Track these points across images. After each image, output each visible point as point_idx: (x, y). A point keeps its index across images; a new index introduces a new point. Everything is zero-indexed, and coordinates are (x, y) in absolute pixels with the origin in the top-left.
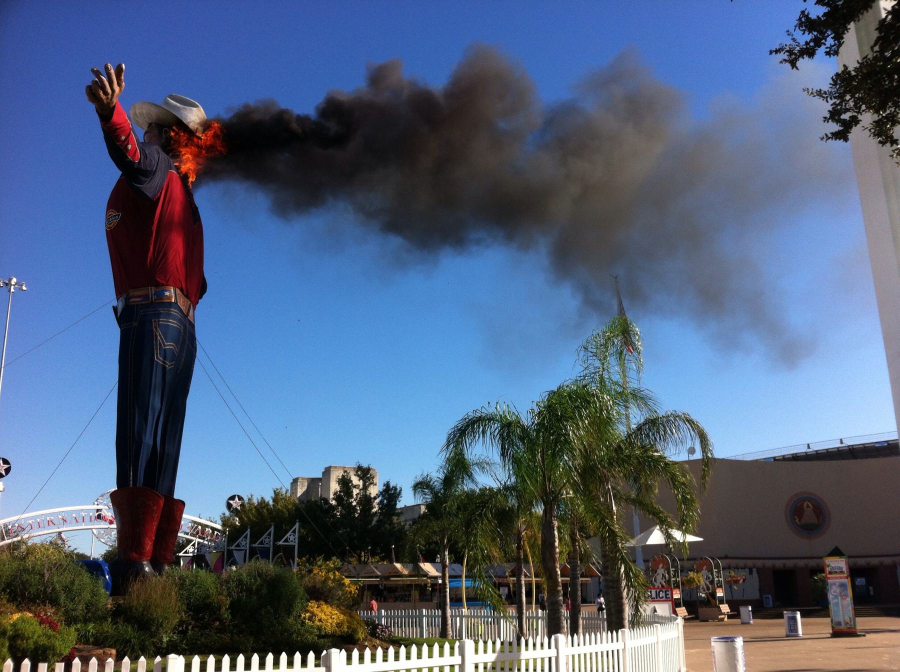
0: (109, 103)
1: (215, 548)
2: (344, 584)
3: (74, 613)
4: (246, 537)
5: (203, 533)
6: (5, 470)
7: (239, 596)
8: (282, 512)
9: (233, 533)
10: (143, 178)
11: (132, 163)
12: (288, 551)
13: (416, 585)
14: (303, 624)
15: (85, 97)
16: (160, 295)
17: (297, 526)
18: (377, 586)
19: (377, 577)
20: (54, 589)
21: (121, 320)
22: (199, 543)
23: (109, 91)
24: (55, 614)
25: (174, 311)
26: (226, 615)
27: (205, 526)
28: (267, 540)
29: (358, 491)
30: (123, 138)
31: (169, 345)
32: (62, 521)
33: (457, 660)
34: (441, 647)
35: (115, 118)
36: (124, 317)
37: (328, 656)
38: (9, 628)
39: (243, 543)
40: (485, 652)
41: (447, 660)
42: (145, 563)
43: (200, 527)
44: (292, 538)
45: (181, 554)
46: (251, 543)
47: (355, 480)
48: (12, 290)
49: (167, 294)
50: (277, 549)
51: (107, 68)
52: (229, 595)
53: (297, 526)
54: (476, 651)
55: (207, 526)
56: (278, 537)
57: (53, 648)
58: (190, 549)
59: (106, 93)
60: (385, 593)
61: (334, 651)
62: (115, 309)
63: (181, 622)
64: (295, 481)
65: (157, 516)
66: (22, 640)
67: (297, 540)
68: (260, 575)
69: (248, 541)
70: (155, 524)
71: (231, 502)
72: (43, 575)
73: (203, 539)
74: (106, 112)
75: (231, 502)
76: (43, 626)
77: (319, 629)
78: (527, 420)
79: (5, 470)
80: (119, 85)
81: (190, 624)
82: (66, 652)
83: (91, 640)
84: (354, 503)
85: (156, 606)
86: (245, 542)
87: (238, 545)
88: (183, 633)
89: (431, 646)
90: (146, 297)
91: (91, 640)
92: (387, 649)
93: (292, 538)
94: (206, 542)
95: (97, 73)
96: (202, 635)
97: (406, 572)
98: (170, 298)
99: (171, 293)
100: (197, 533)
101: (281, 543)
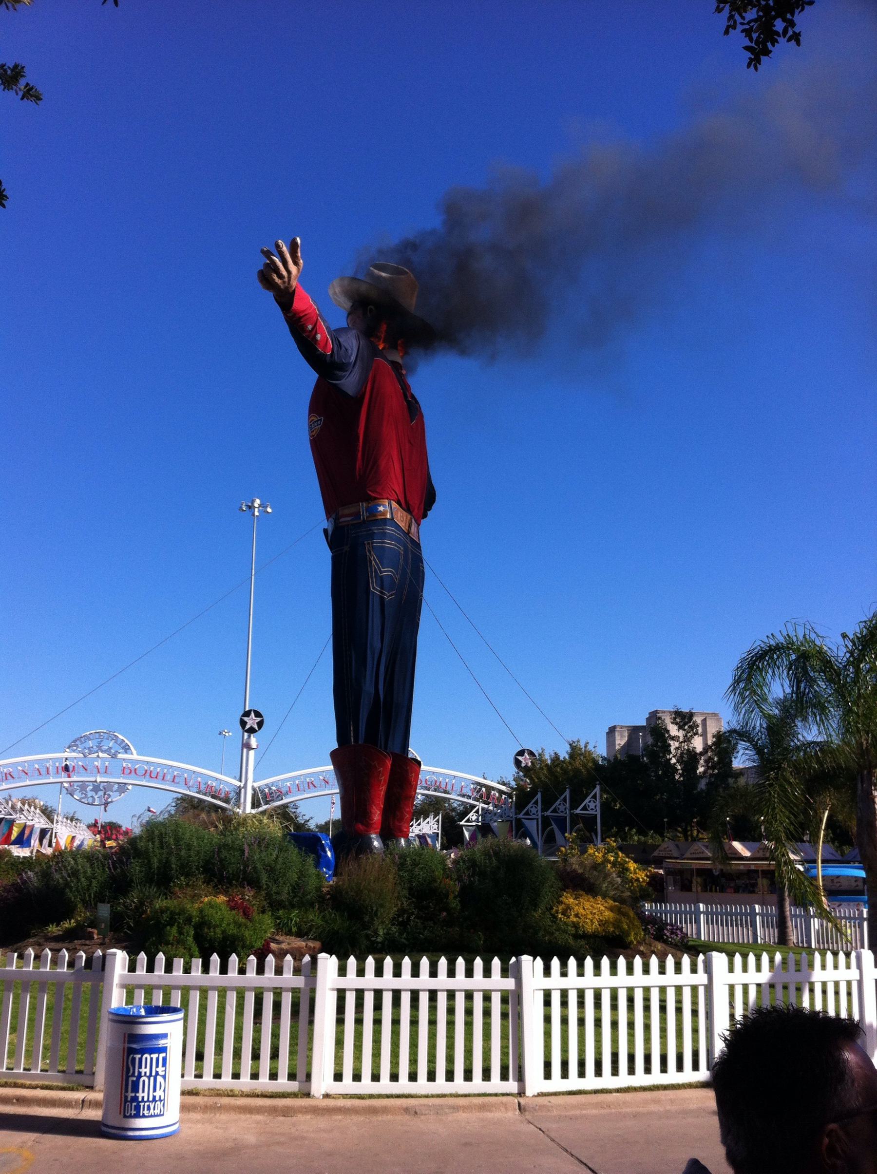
0: (287, 288)
1: (501, 817)
2: (627, 869)
3: (278, 898)
4: (536, 803)
5: (488, 797)
6: (258, 723)
7: (470, 880)
8: (581, 772)
9: (522, 797)
10: (340, 373)
11: (324, 355)
12: (590, 822)
13: (763, 872)
14: (555, 917)
15: (258, 285)
16: (373, 511)
17: (597, 789)
18: (710, 870)
19: (707, 859)
20: (255, 868)
21: (332, 544)
22: (483, 809)
23: (285, 273)
24: (254, 897)
25: (389, 529)
26: (454, 904)
27: (489, 788)
28: (562, 807)
29: (677, 744)
30: (310, 327)
31: (387, 572)
32: (323, 783)
33: (701, 978)
34: (564, 964)
35: (297, 305)
36: (336, 539)
37: (518, 963)
38: (195, 913)
39: (534, 810)
40: (836, 967)
41: (686, 978)
42: (373, 836)
43: (484, 789)
44: (593, 805)
45: (462, 823)
46: (543, 810)
47: (673, 730)
48: (257, 513)
49: (381, 508)
50: (575, 819)
51: (278, 246)
52: (460, 879)
53: (597, 789)
54: (731, 970)
55: (493, 789)
56: (574, 805)
57: (242, 939)
58: (472, 816)
59: (281, 276)
60: (723, 880)
61: (526, 959)
62: (325, 531)
63: (402, 912)
64: (612, 730)
65: (384, 779)
66: (209, 928)
67: (598, 808)
68: (496, 854)
69: (568, 805)
70: (383, 789)
71: (520, 758)
72: (243, 851)
73: (488, 804)
74: (285, 298)
75: (520, 758)
76: (234, 912)
77: (575, 926)
78: (838, 649)
79: (258, 723)
80: (296, 263)
81: (413, 913)
82: (259, 944)
83: (294, 929)
84: (673, 761)
85: (369, 891)
86: (535, 809)
87: (527, 813)
88: (404, 925)
89: (745, 956)
90: (357, 515)
91: (294, 929)
92: (761, 956)
93: (593, 805)
94: (491, 808)
95: (268, 254)
96: (425, 928)
97: (747, 854)
98: (384, 513)
99: (386, 508)
100: (481, 796)
101: (578, 811)
